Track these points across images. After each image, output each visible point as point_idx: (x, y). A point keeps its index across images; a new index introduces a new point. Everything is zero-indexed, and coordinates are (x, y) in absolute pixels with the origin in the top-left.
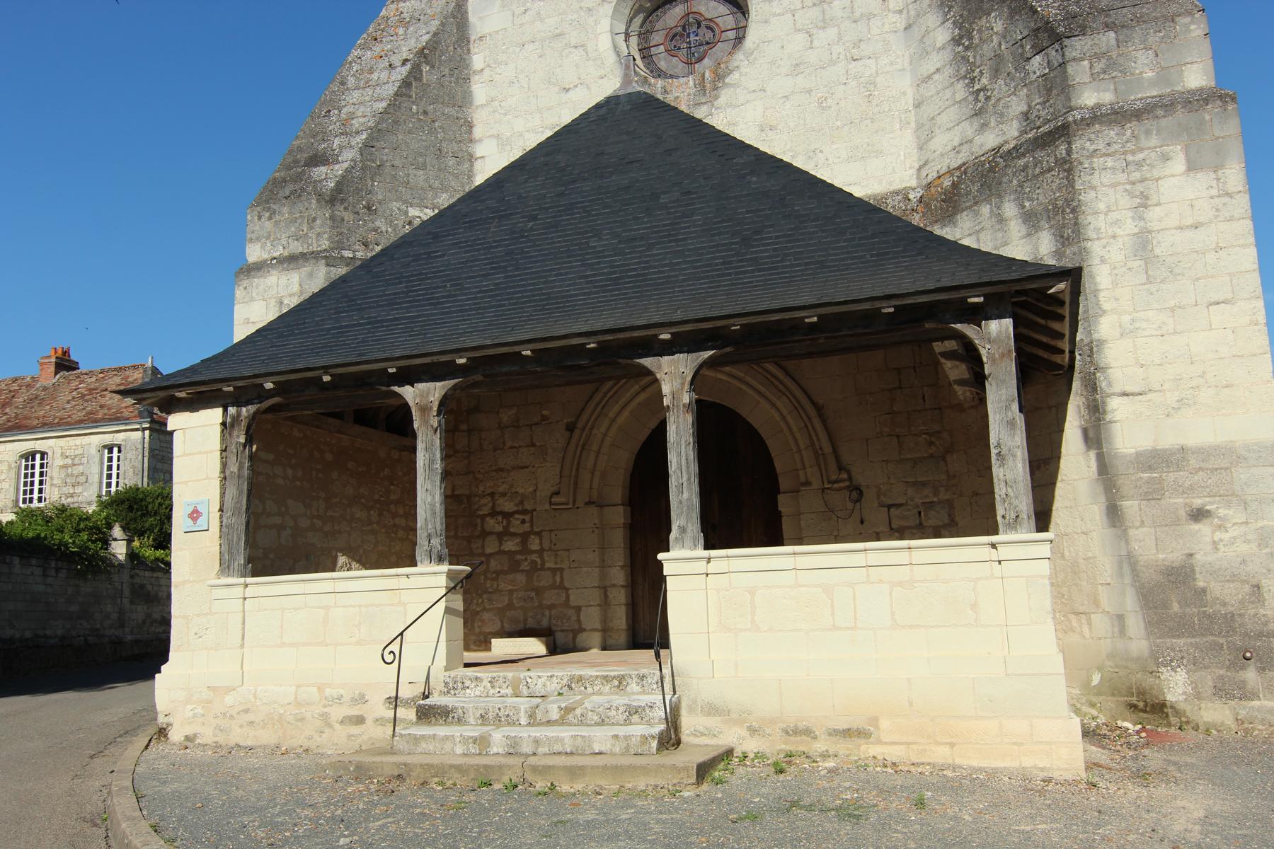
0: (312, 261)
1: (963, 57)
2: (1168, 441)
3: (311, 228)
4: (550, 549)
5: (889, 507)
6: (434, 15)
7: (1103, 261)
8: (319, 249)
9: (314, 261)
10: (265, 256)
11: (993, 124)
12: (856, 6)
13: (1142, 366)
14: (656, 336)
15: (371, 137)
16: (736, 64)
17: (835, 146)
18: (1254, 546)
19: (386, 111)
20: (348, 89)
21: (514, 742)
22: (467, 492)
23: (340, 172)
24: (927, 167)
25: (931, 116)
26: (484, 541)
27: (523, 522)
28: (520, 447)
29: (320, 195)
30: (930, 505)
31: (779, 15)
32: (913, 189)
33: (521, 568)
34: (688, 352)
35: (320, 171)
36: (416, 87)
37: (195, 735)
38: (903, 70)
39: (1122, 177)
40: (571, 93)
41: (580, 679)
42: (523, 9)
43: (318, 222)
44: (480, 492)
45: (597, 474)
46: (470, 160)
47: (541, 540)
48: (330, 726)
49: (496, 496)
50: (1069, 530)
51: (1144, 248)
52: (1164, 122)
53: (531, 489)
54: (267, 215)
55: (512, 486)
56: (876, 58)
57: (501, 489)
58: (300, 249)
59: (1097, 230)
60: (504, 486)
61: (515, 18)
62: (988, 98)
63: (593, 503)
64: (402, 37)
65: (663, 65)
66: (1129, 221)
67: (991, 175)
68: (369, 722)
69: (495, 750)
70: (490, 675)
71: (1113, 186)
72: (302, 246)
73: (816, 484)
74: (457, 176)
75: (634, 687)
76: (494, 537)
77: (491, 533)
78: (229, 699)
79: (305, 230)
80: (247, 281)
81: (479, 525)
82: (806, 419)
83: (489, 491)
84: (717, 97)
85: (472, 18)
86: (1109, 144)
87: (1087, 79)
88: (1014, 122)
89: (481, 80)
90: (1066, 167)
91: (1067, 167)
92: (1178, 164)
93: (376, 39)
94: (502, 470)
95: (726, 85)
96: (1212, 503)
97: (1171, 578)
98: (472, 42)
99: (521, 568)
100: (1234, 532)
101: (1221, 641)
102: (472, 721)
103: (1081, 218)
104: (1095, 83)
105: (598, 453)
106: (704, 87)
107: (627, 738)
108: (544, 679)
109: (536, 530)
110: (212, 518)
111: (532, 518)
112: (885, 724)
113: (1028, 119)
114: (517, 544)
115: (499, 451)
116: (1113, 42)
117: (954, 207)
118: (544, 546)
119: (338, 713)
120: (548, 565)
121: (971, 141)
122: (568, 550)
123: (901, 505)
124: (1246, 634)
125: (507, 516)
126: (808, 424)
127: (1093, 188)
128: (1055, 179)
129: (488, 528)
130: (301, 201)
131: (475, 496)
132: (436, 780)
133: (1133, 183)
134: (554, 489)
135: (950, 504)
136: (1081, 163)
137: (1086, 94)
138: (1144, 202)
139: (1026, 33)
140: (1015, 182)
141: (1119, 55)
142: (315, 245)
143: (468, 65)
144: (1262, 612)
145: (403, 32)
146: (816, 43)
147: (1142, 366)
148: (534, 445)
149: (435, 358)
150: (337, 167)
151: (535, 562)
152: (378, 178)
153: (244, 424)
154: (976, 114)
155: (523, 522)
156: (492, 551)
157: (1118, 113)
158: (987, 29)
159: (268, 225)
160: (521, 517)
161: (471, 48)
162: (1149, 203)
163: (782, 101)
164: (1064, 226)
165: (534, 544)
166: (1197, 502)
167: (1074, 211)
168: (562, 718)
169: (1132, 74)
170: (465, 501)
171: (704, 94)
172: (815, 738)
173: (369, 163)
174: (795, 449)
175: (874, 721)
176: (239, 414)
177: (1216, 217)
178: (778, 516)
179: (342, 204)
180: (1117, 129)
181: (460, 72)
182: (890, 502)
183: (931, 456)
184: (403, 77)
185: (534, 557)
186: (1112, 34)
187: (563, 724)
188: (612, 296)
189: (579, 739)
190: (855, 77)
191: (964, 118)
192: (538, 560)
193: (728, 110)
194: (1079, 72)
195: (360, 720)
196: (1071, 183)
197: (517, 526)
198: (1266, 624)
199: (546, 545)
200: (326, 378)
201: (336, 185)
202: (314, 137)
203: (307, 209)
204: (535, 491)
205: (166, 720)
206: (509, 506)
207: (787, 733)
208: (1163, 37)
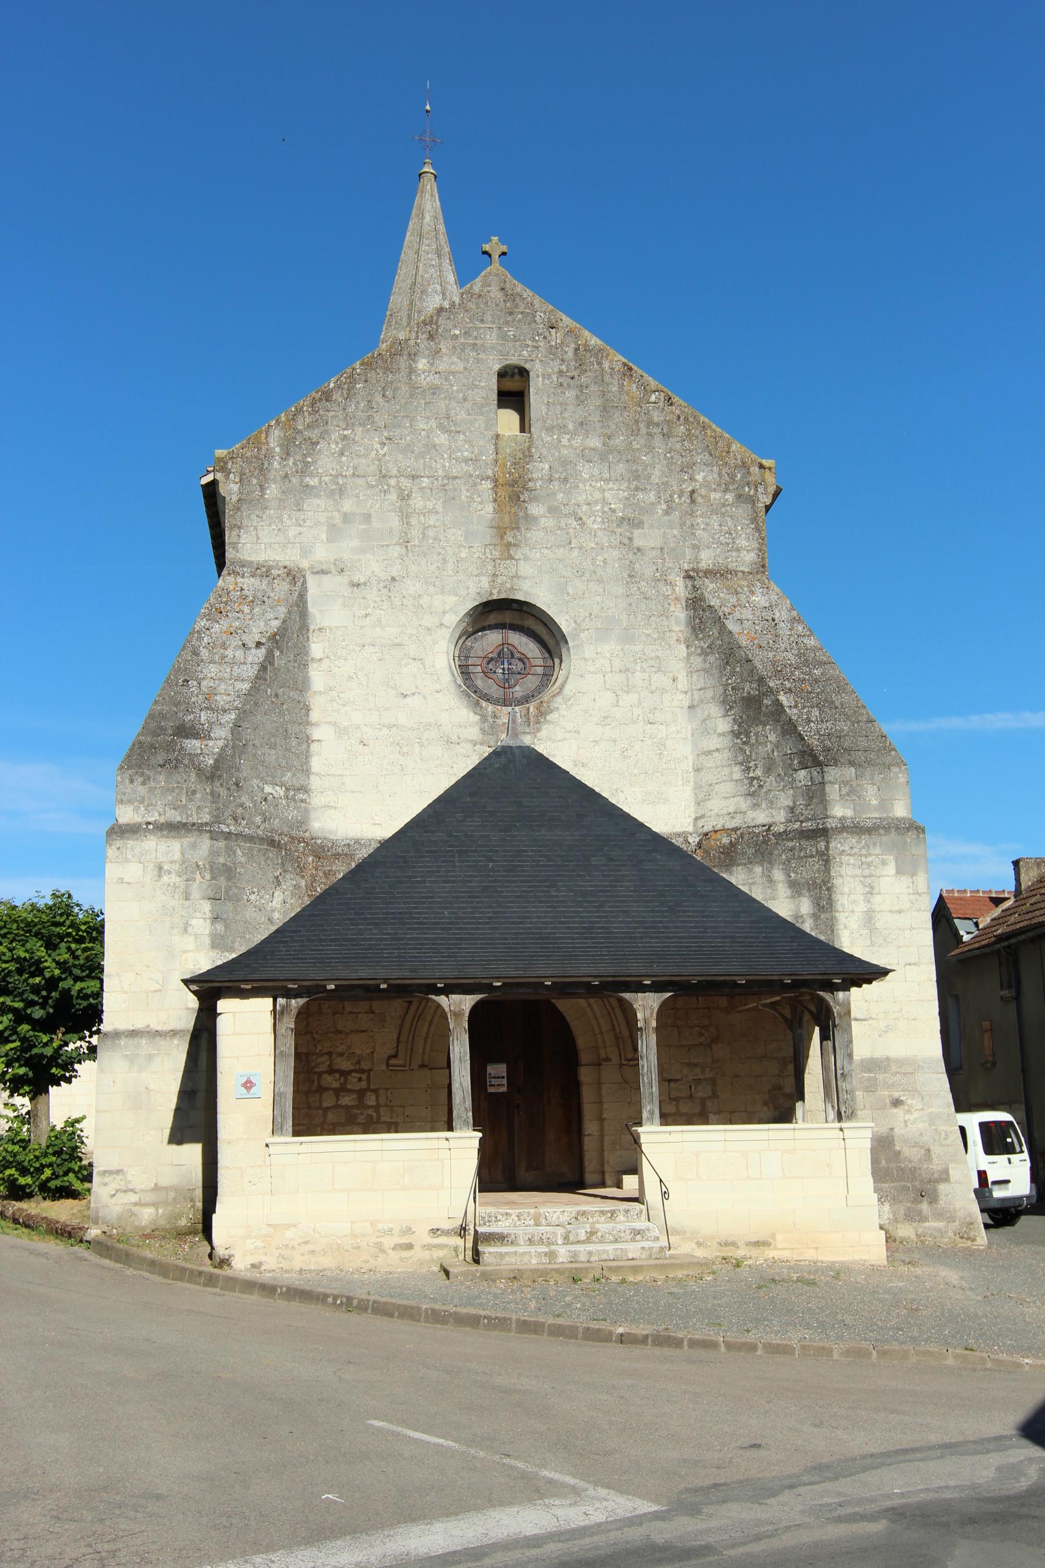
0: (196, 833)
1: (740, 749)
2: (879, 1054)
3: (191, 800)
4: (386, 1105)
5: (669, 1081)
6: (278, 601)
7: (846, 927)
8: (199, 821)
9: (198, 833)
10: (138, 819)
11: (763, 806)
12: (653, 680)
13: (866, 1001)
14: (641, 981)
15: (239, 718)
16: (555, 706)
17: (633, 789)
18: (927, 1124)
19: (249, 694)
20: (202, 661)
21: (575, 1255)
22: (306, 1051)
23: (217, 750)
24: (703, 820)
25: (710, 782)
26: (321, 1095)
27: (360, 1080)
28: (359, 1013)
29: (200, 771)
30: (698, 1081)
31: (592, 673)
32: (691, 834)
33: (358, 1121)
34: (655, 992)
35: (193, 745)
36: (270, 671)
37: (261, 1263)
38: (686, 739)
39: (858, 872)
40: (408, 700)
41: (584, 1213)
42: (364, 612)
43: (198, 795)
44: (317, 1051)
45: (429, 1040)
46: (307, 741)
47: (377, 1097)
48: (383, 1251)
49: (334, 1056)
50: (813, 1108)
51: (870, 922)
52: (884, 839)
53: (369, 1051)
54: (140, 779)
55: (350, 1048)
56: (667, 726)
57: (339, 1050)
58: (179, 819)
59: (843, 905)
60: (343, 1046)
61: (356, 619)
62: (760, 786)
63: (426, 1066)
64: (249, 617)
65: (479, 683)
66: (862, 902)
67: (764, 846)
68: (417, 1248)
69: (561, 1260)
70: (517, 1211)
71: (854, 876)
72: (180, 816)
73: (615, 1060)
74: (298, 756)
75: (621, 1217)
76: (331, 1092)
77: (328, 1089)
78: (290, 1234)
79: (184, 800)
80: (121, 842)
81: (316, 1081)
82: (609, 1008)
83: (326, 1050)
84: (539, 730)
85: (312, 609)
86: (851, 848)
87: (838, 798)
88: (782, 811)
89: (320, 669)
90: (825, 858)
91: (826, 859)
92: (891, 869)
93: (221, 612)
94: (341, 1032)
95: (547, 722)
96: (904, 1096)
97: (882, 1144)
98: (311, 631)
99: (358, 1121)
100: (916, 1115)
101: (909, 1185)
102: (522, 1242)
103: (833, 895)
104: (842, 801)
105: (431, 1023)
106: (529, 719)
107: (650, 1248)
108: (558, 1213)
109: (372, 1087)
110: (265, 1089)
111: (369, 1076)
112: (779, 1237)
113: (793, 812)
114: (353, 1100)
115: (338, 1015)
116: (854, 775)
117: (731, 860)
118: (380, 1102)
119: (388, 1242)
120: (383, 1119)
121: (744, 813)
122: (403, 1107)
123: (676, 1081)
124: (922, 1181)
125: (345, 1074)
126: (611, 1012)
127: (841, 876)
128: (816, 864)
129: (324, 1084)
130: (179, 772)
131: (313, 1054)
132: (541, 1279)
133: (865, 877)
134: (393, 1052)
135: (713, 1082)
136: (835, 858)
137: (836, 808)
138: (871, 891)
139: (794, 751)
140: (784, 857)
141: (857, 785)
142: (195, 817)
143: (307, 652)
144: (931, 1166)
145: (249, 611)
146: (621, 703)
147: (866, 1001)
148: (373, 1012)
149: (478, 981)
150: (211, 743)
151: (372, 1116)
152: (244, 757)
153: (294, 1012)
154: (750, 795)
155: (360, 1080)
156: (329, 1105)
157: (857, 827)
158: (763, 736)
159: (142, 790)
160: (358, 1075)
161: (311, 637)
162: (874, 892)
163: (592, 744)
164: (820, 898)
165: (371, 1100)
166: (896, 1095)
167: (828, 889)
168: (588, 1238)
169: (865, 800)
170: (304, 1058)
171: (529, 725)
172: (738, 1247)
173: (237, 745)
174: (597, 1031)
175: (773, 1236)
176: (288, 1005)
177: (912, 907)
178: (577, 1084)
179: (219, 780)
180: (857, 838)
181: (301, 659)
182: (669, 1077)
183: (701, 1044)
184: (261, 660)
185: (370, 1111)
186: (853, 769)
187: (589, 1243)
188: (593, 943)
189: (619, 1250)
190: (650, 737)
191: (739, 793)
192: (374, 1115)
193: (548, 743)
194: (833, 791)
195: (409, 1247)
196: (827, 871)
197: (353, 1082)
198: (933, 1174)
199: (382, 1100)
200: (383, 986)
201: (215, 763)
202: (176, 705)
203: (185, 781)
204: (372, 1053)
205: (227, 1252)
206: (345, 1065)
207: (721, 1245)
208: (883, 779)
